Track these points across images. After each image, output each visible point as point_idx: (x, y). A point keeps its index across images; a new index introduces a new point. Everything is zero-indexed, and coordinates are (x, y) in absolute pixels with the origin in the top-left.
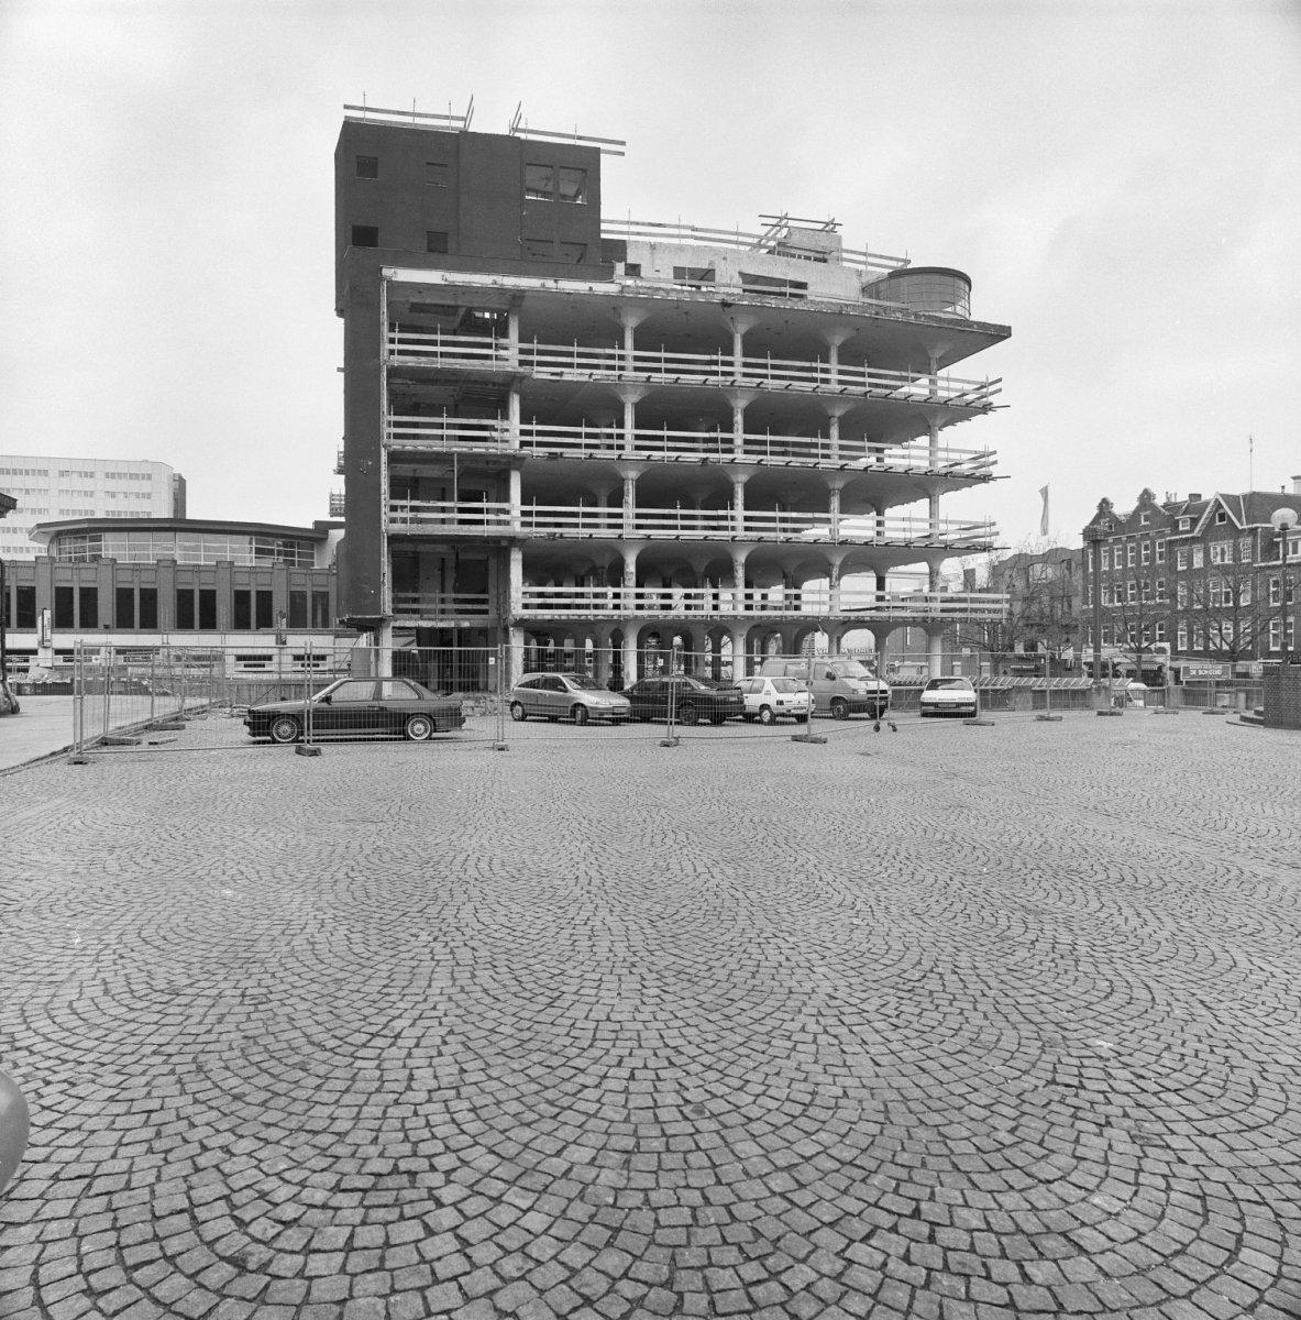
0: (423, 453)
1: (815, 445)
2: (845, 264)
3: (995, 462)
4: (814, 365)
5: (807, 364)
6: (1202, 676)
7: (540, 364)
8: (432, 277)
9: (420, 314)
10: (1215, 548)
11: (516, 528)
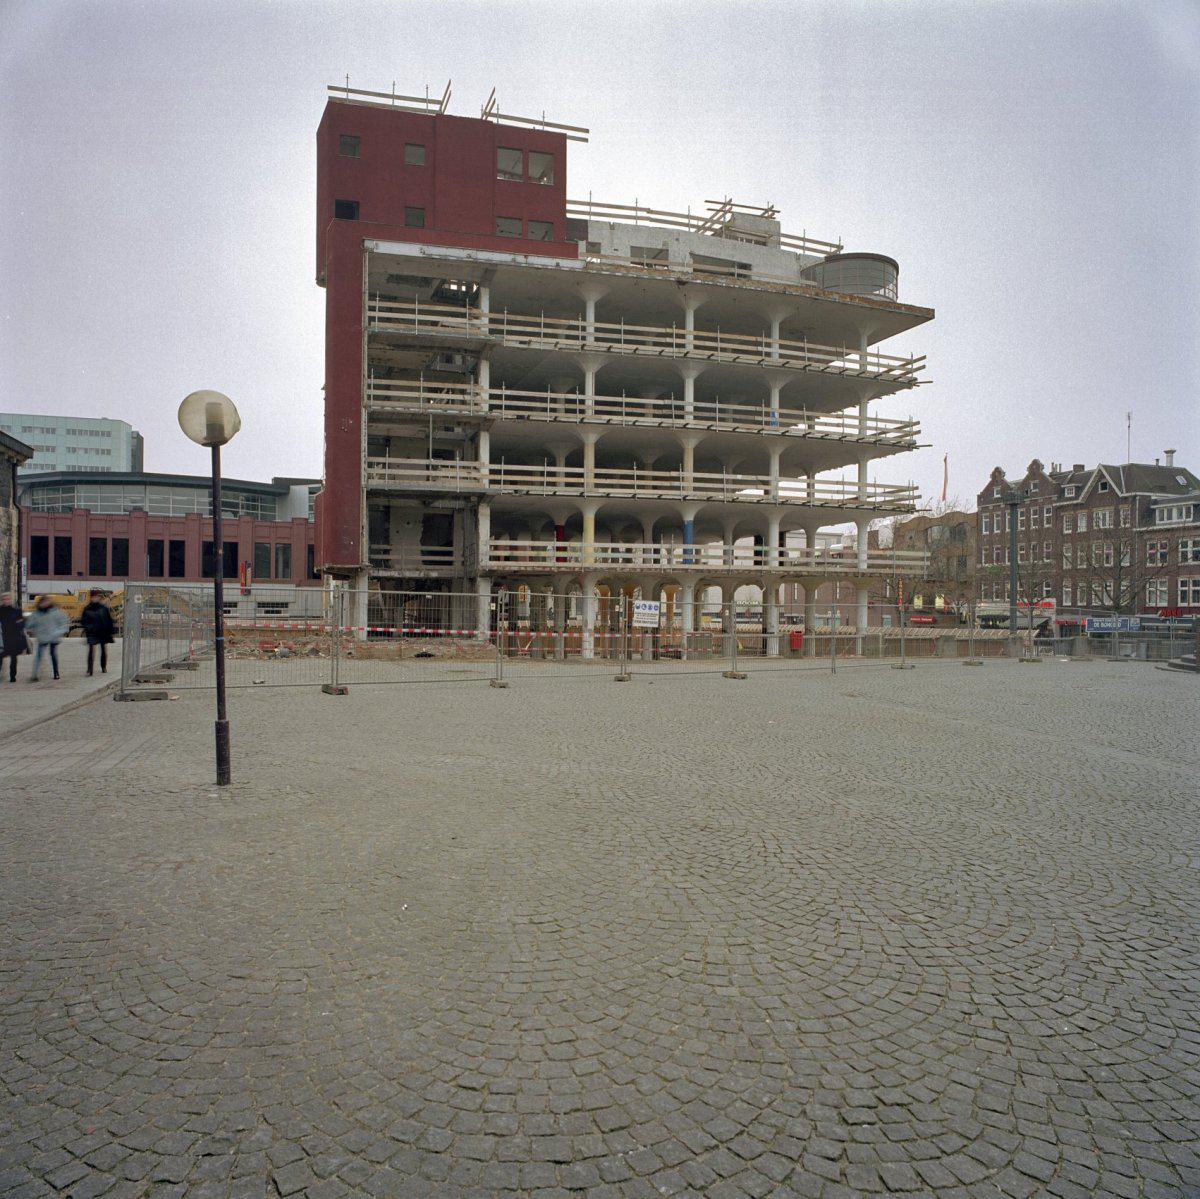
0: (399, 413)
1: (759, 413)
2: (783, 248)
3: (919, 432)
4: (759, 339)
5: (753, 339)
6: (1108, 628)
7: (510, 333)
8: (411, 250)
9: (403, 283)
10: (1099, 512)
11: (485, 485)
